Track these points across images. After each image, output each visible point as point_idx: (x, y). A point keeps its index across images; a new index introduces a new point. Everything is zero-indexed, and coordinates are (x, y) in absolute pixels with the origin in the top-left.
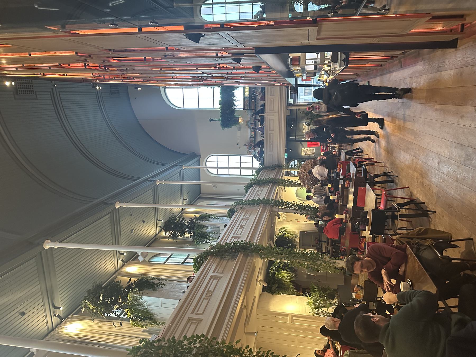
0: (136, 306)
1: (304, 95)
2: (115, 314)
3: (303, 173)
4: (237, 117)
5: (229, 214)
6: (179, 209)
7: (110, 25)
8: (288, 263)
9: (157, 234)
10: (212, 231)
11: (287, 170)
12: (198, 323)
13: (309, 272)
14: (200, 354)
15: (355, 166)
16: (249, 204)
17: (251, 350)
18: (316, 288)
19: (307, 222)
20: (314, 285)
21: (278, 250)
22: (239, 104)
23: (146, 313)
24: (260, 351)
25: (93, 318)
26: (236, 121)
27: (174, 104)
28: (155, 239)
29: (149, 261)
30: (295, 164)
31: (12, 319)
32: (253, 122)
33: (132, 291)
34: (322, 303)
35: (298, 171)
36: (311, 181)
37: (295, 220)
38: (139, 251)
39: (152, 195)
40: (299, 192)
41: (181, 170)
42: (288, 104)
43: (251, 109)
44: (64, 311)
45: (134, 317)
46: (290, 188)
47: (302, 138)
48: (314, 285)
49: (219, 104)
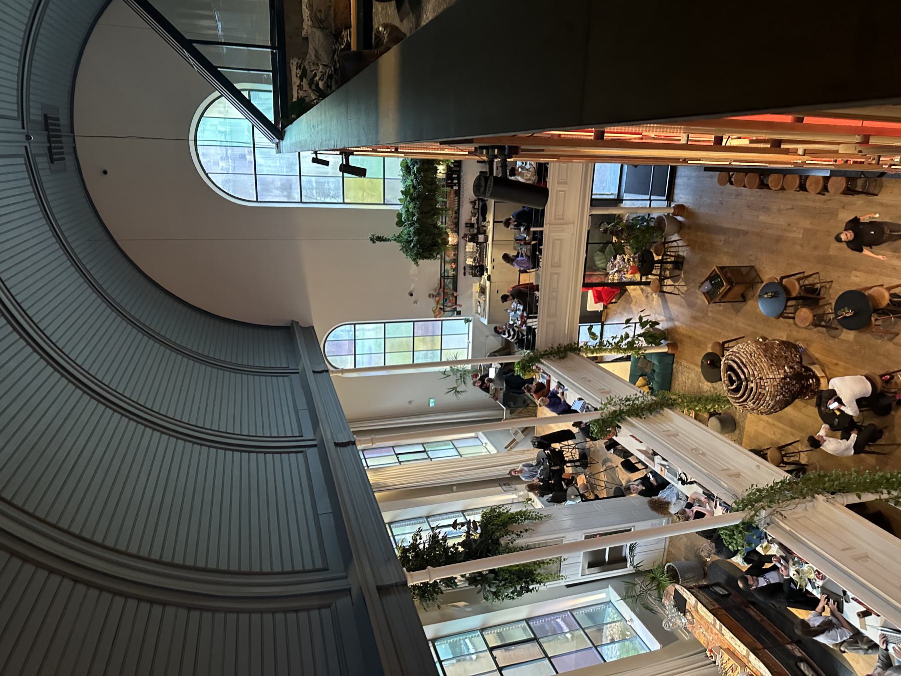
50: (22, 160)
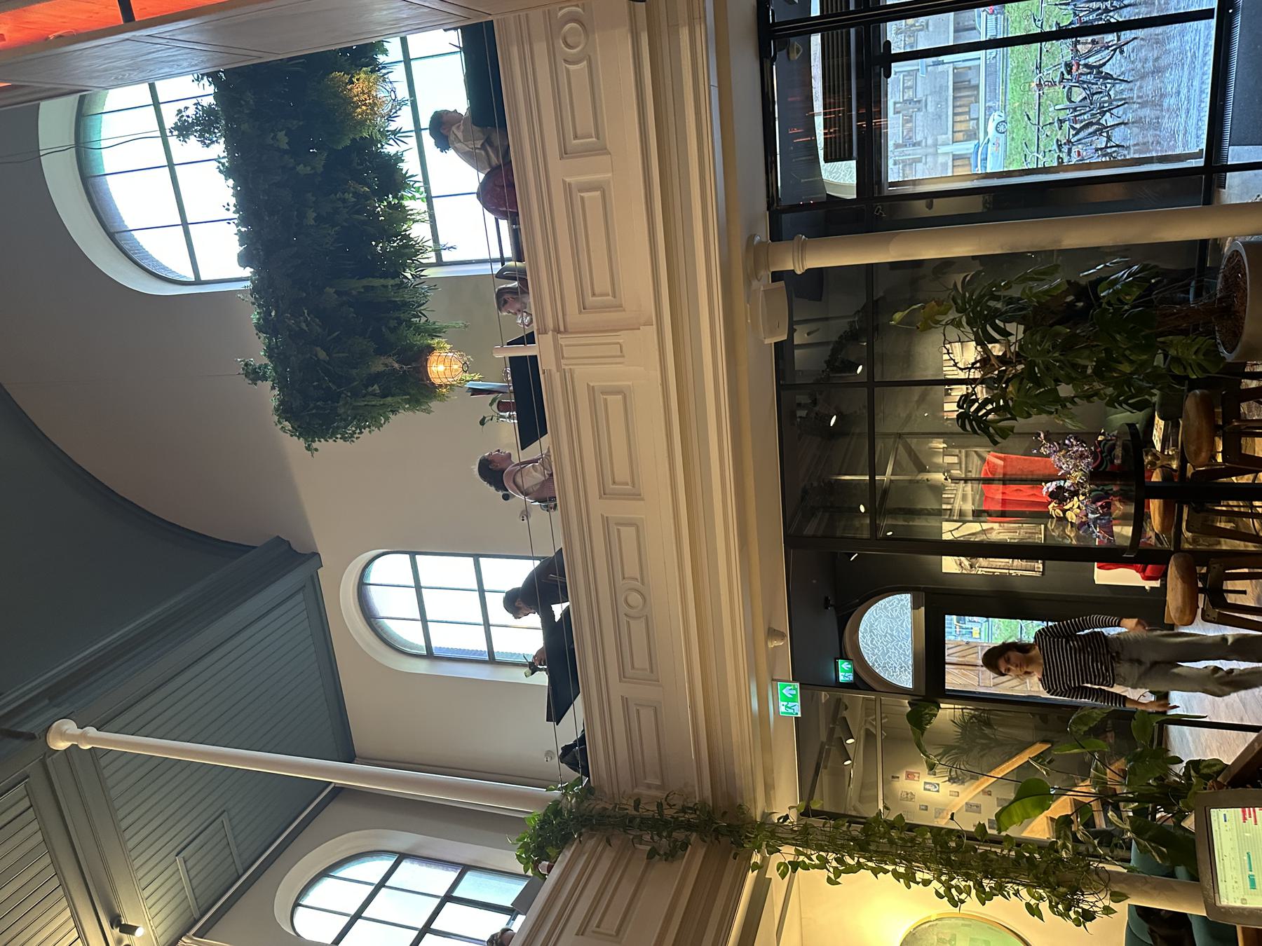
1: (953, 142)
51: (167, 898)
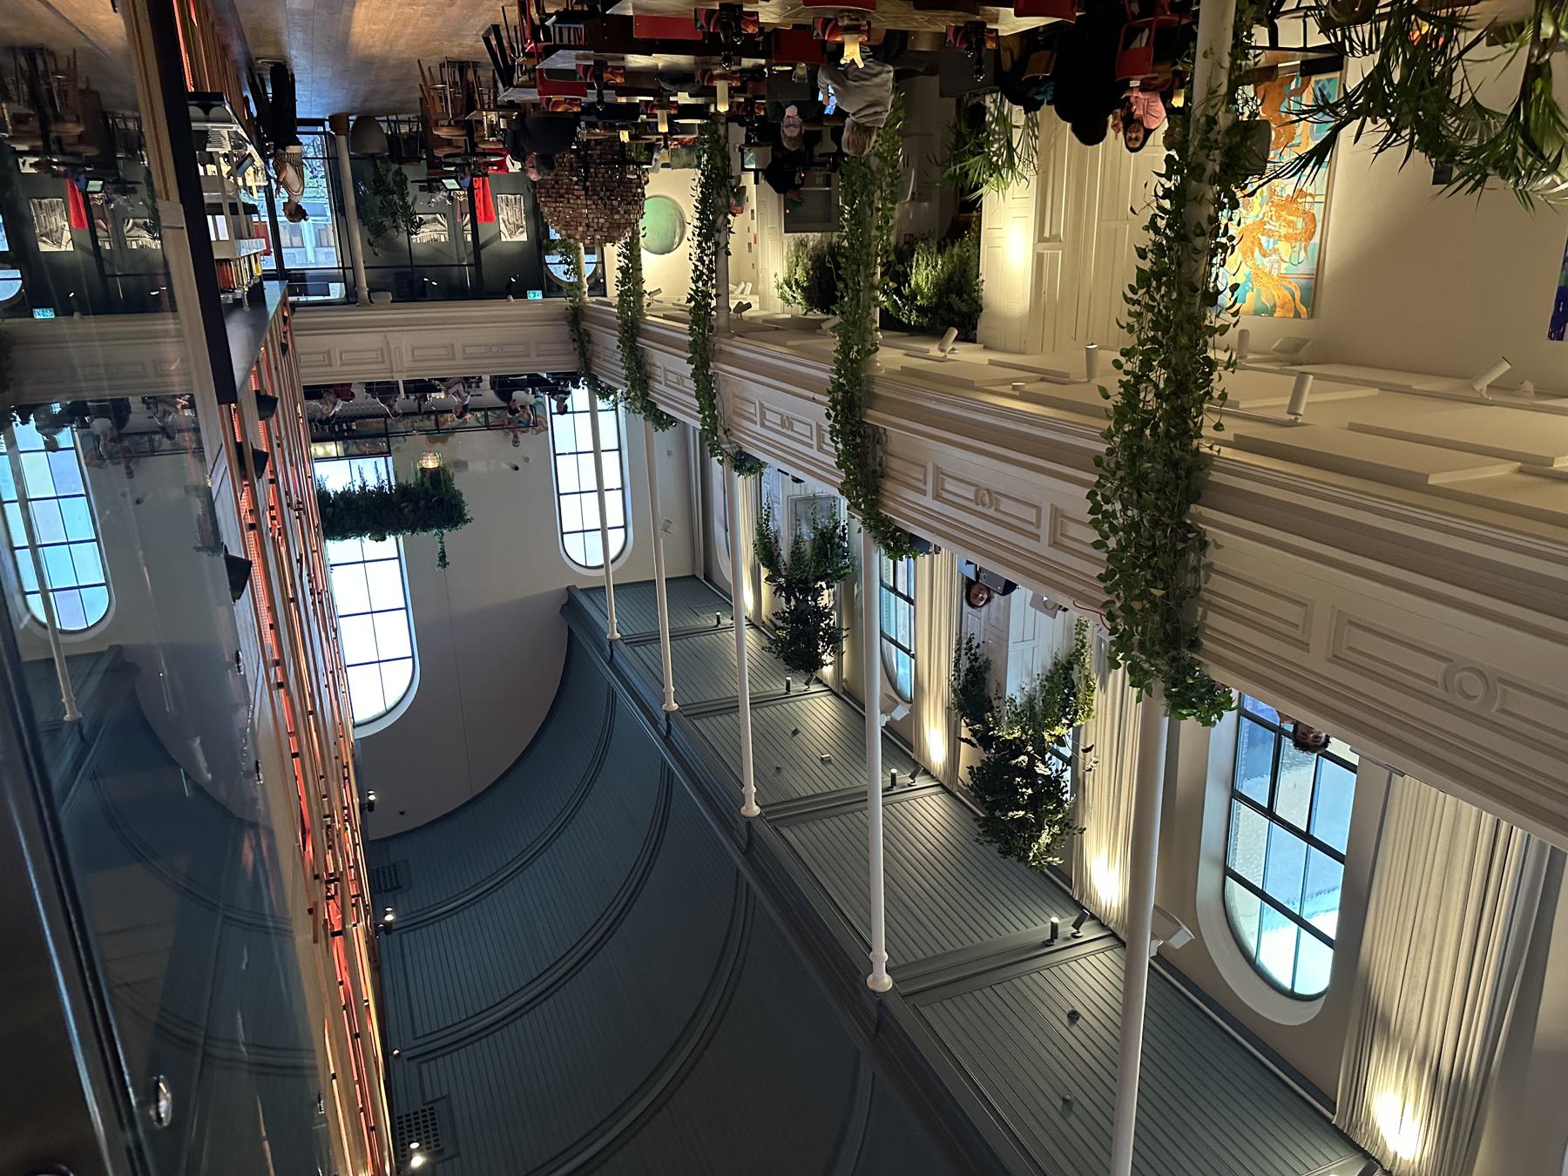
0: (1035, 714)
2: (1062, 771)
3: (591, 229)
4: (419, 475)
5: (749, 470)
6: (749, 635)
7: (259, 780)
8: (883, 265)
9: (830, 690)
10: (808, 524)
11: (586, 290)
12: (1062, 516)
13: (904, 191)
14: (1140, 495)
15: (549, 51)
16: (713, 407)
17: (1124, 353)
18: (953, 168)
19: (752, 211)
20: (945, 175)
21: (846, 299)
22: (371, 473)
23: (1052, 681)
24: (1128, 324)
25: (1076, 832)
26: (437, 478)
27: (401, 694)
28: (846, 693)
29: (910, 703)
30: (560, 263)
31: (1089, 1041)
32: (429, 418)
33: (993, 729)
34: (996, 146)
35: (583, 248)
36: (615, 203)
37: (750, 251)
38: (880, 721)
39: (712, 719)
40: (656, 244)
41: (626, 644)
42: (351, 300)
43: (386, 429)
44: (1063, 913)
45: (1065, 716)
46: (645, 274)
47: (466, 242)
48: (945, 175)
49: (384, 539)
50: (405, 937)
51: (1285, 1141)
